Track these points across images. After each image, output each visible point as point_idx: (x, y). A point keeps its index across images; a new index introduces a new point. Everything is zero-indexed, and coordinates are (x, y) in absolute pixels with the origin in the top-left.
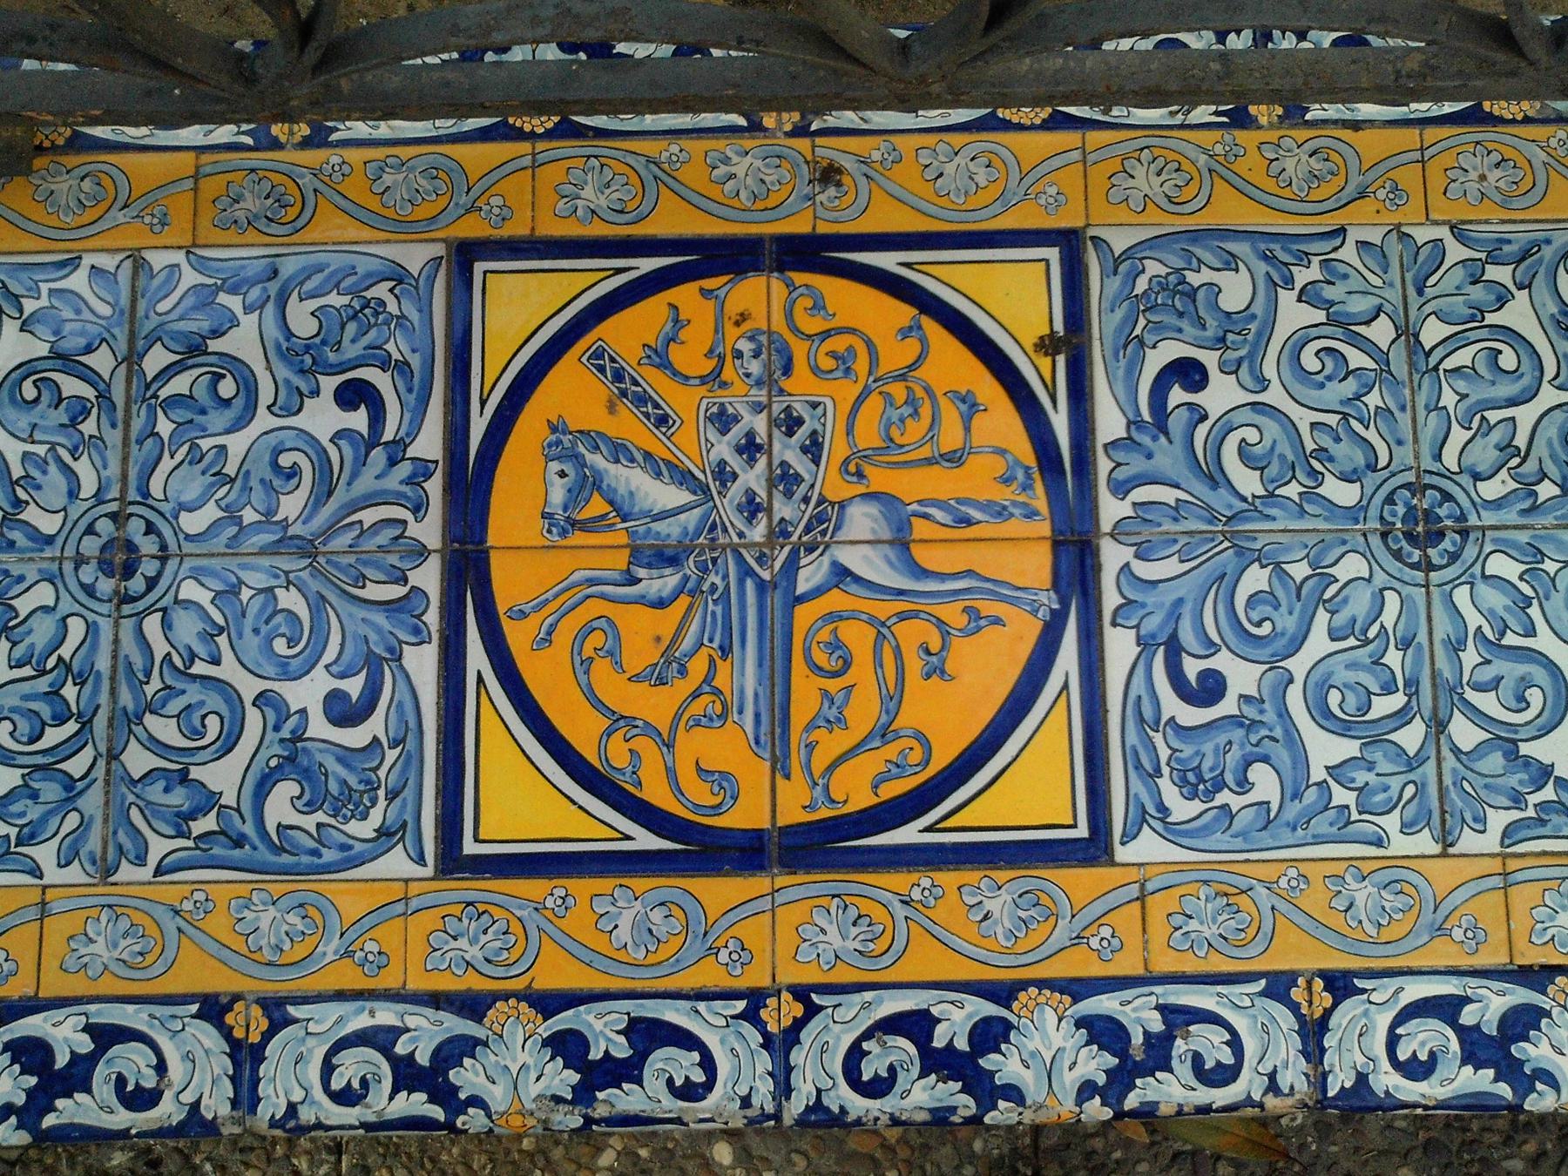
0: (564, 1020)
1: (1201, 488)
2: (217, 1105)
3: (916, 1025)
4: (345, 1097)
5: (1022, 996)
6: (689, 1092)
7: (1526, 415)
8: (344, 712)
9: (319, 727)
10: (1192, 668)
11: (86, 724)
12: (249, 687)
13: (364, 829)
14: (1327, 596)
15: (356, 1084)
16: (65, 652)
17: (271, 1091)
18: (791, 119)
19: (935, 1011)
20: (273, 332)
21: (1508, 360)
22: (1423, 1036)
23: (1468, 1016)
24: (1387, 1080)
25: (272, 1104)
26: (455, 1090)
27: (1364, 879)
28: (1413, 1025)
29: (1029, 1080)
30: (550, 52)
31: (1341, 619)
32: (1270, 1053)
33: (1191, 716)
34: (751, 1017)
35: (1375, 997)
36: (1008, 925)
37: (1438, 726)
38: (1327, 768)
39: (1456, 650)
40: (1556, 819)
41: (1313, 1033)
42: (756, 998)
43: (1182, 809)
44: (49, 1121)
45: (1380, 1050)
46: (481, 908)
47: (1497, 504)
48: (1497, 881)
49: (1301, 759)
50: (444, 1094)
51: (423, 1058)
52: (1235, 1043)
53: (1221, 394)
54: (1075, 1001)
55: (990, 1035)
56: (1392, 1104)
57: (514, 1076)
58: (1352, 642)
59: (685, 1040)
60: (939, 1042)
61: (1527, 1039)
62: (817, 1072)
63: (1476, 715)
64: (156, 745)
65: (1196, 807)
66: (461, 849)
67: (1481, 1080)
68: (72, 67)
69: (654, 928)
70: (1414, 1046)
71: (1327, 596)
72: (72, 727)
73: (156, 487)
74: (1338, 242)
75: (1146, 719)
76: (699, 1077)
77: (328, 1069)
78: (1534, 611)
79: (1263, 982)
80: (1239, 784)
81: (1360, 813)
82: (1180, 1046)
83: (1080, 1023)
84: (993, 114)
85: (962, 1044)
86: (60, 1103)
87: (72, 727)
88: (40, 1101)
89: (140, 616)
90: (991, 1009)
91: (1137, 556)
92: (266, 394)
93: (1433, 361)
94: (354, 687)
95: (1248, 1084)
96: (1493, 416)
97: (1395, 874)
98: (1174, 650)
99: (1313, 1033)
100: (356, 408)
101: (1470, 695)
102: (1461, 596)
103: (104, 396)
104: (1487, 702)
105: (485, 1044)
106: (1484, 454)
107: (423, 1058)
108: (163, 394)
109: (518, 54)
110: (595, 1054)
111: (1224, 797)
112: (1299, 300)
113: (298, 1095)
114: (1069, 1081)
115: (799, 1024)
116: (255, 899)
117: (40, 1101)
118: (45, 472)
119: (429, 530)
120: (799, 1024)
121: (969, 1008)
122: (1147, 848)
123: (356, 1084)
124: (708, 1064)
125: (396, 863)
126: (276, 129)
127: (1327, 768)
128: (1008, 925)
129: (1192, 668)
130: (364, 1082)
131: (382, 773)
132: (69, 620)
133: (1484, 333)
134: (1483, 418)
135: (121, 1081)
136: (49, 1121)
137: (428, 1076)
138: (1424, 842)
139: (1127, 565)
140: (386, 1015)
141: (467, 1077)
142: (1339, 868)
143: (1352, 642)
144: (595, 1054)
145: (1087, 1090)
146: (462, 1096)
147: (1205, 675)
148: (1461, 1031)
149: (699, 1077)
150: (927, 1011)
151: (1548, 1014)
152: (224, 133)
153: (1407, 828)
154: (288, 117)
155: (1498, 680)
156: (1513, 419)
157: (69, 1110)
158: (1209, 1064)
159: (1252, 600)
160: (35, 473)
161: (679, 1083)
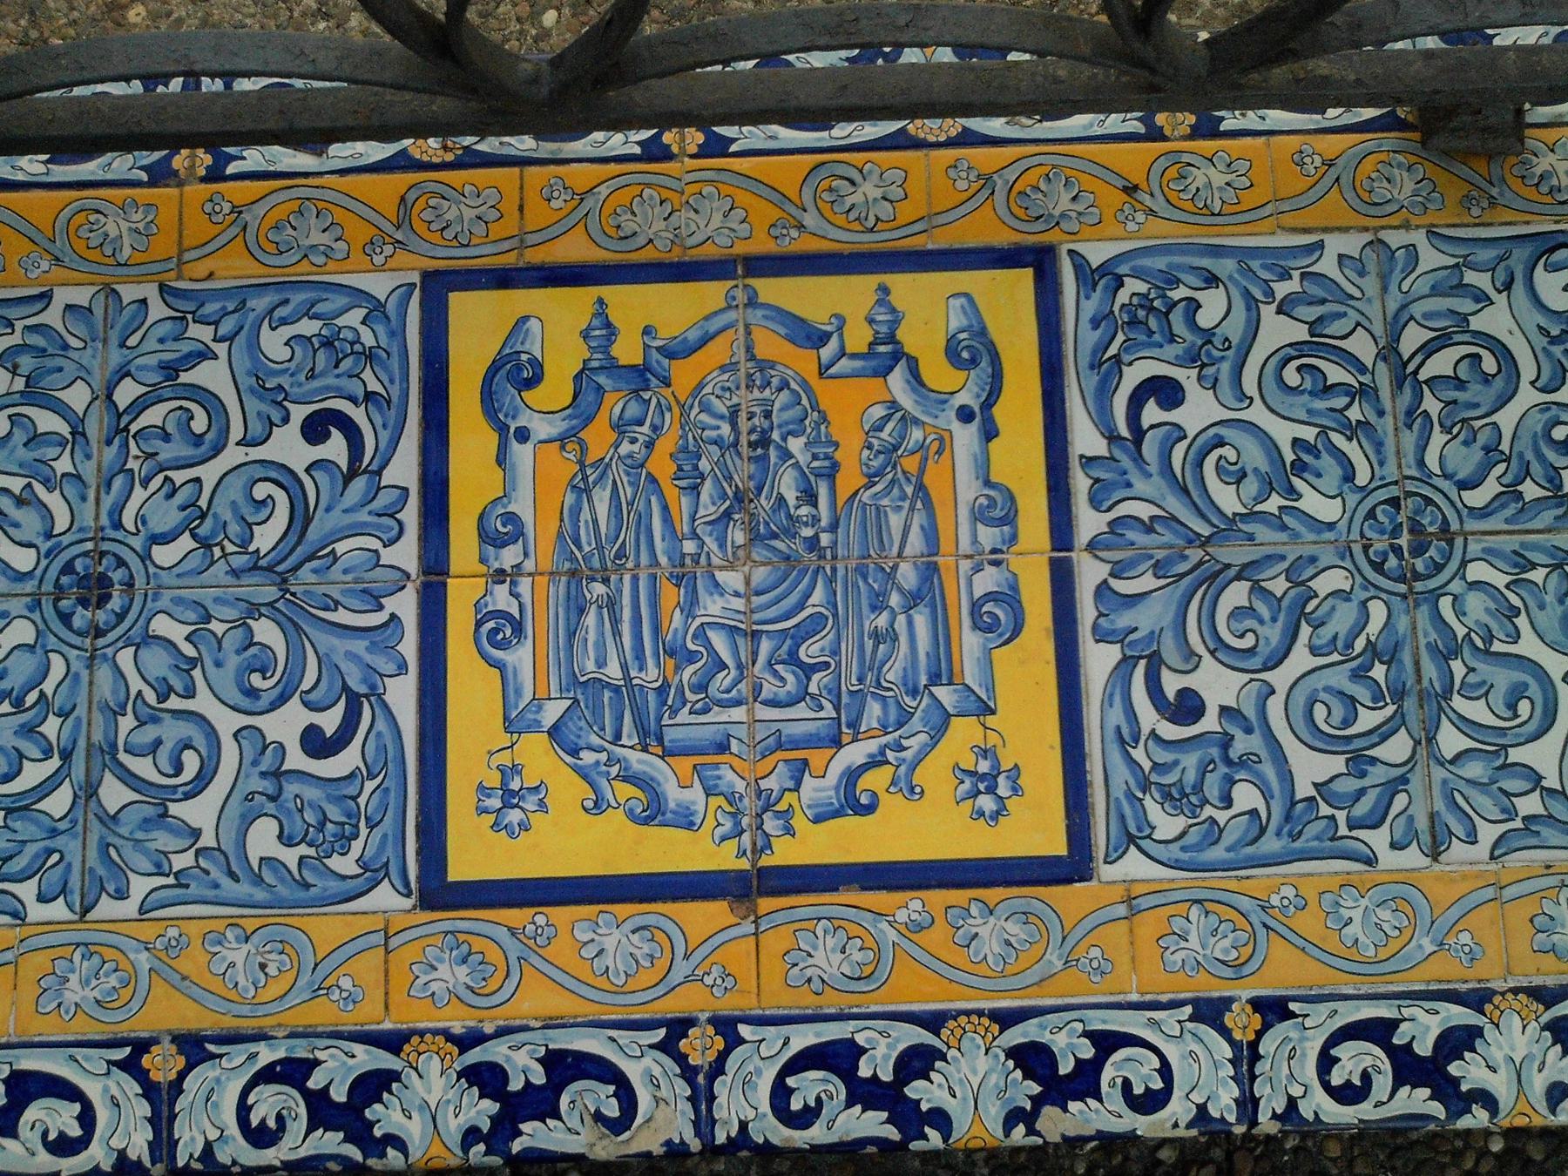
0: (475, 1056)
1: (1175, 505)
2: (1224, 1103)
3: (837, 1058)
4: (1348, 1094)
5: (951, 1024)
6: (63, 1146)
7: (209, 473)
8: (317, 744)
9: (296, 759)
10: (1171, 684)
11: (66, 756)
12: (226, 722)
13: (345, 864)
14: (1308, 610)
15: (272, 1124)
16: (48, 687)
17: (1268, 1090)
18: (694, 138)
19: (860, 1039)
20: (242, 363)
21: (199, 424)
22: (1354, 1059)
23: (315, 1082)
24: (1319, 1105)
25: (188, 1146)
26: (1455, 1082)
27: (247, 940)
28: (1341, 1051)
29: (1500, 1085)
30: (945, 55)
31: (1326, 633)
32: (1204, 1080)
33: (1170, 731)
34: (131, 1066)
35: (1308, 1023)
36: (997, 949)
37: (90, 791)
38: (1315, 785)
39: (1447, 659)
40: (1550, 834)
41: (1247, 1058)
42: (679, 1027)
43: (1167, 825)
44: (516, 1146)
45: (229, 1117)
46: (837, 923)
47: (1483, 513)
48: (1122, 910)
49: (1287, 778)
50: (360, 1133)
51: (339, 1095)
52: (1165, 1071)
53: (1199, 410)
54: (1547, 1008)
55: (917, 1063)
56: (1336, 1133)
57: (973, 1092)
58: (1335, 657)
59: (65, 1090)
60: (864, 1071)
61: (380, 1101)
62: (743, 1103)
63: (129, 779)
64: (1465, 725)
65: (1180, 823)
66: (1057, 859)
67: (872, 1124)
68: (1027, 57)
69: (1013, 940)
70: (262, 1114)
71: (1308, 610)
72: (55, 762)
73: (128, 520)
74: (39, 306)
75: (1127, 738)
76: (75, 1131)
77: (1326, 1062)
78: (1522, 621)
79: (128, 1049)
80: (1222, 799)
81: (1351, 828)
82: (1108, 1073)
83: (1012, 1053)
84: (1392, 113)
85: (886, 1076)
86: (525, 1127)
87: (55, 762)
88: (505, 1126)
89: (1435, 595)
90: (924, 1037)
91: (1112, 575)
92: (1528, 370)
93: (1411, 368)
94: (330, 721)
95: (1178, 1110)
96: (179, 477)
97: (1401, 894)
98: (1155, 664)
99: (1247, 1058)
100: (328, 435)
101: (123, 757)
102: (125, 658)
103: (78, 432)
104: (143, 767)
105: (944, 1058)
106: (166, 516)
107: (339, 1095)
108: (134, 428)
109: (911, 56)
110: (516, 1085)
111: (1208, 811)
112: (1279, 312)
113: (213, 1134)
114: (454, 1126)
115: (723, 1057)
116: (229, 934)
117: (505, 1126)
118: (1317, 457)
119: (406, 554)
120: (723, 1057)
121: (1443, 1014)
122: (1134, 865)
123: (272, 1124)
124: (87, 1118)
125: (385, 897)
126: (1161, 119)
127: (1315, 785)
128: (997, 949)
129: (1171, 684)
130: (280, 1118)
131: (362, 800)
132: (1370, 604)
133: (1466, 337)
134: (166, 478)
135: (1127, 1085)
136: (516, 1146)
137: (347, 1114)
138: (1413, 857)
139: (1105, 581)
140: (1383, 1011)
141: (386, 1116)
142: (219, 925)
143: (1335, 657)
144: (516, 1085)
145: (471, 1135)
146: (377, 1132)
147: (1184, 693)
148: (308, 1095)
149: (75, 1131)
150: (852, 1042)
151: (944, 1058)
152: (1115, 123)
153: (42, 899)
154: (1174, 107)
155: (158, 743)
156: (307, 470)
157: (534, 1135)
158: (1138, 1090)
159: (1236, 613)
160: (1306, 458)
161: (52, 1136)
